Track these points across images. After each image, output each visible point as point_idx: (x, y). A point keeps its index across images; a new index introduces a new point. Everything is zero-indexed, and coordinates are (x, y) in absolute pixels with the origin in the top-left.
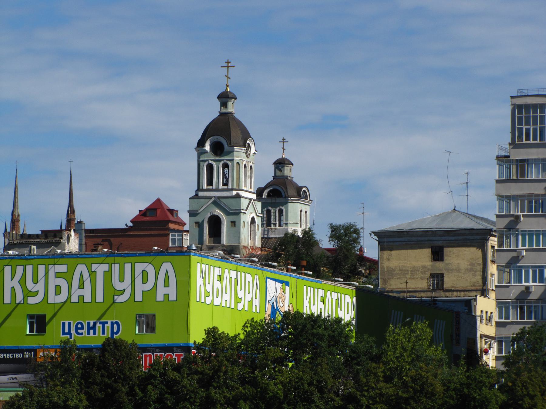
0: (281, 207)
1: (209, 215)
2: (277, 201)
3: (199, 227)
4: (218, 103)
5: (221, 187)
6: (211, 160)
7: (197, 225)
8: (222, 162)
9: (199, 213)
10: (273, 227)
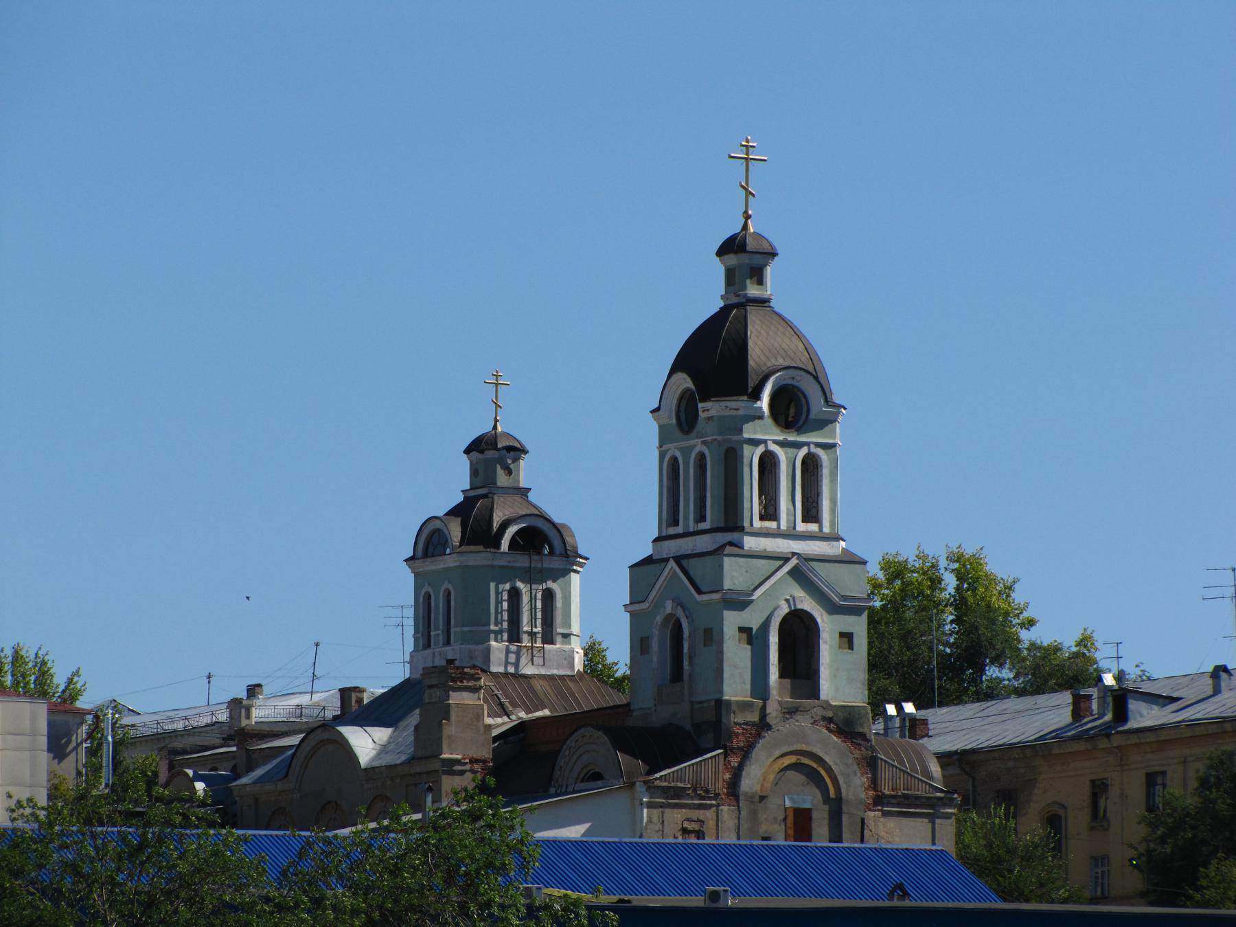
0: (550, 584)
1: (785, 609)
2: (545, 566)
3: (750, 642)
4: (717, 271)
5: (801, 527)
6: (775, 442)
7: (745, 636)
8: (804, 451)
9: (752, 601)
10: (526, 641)
